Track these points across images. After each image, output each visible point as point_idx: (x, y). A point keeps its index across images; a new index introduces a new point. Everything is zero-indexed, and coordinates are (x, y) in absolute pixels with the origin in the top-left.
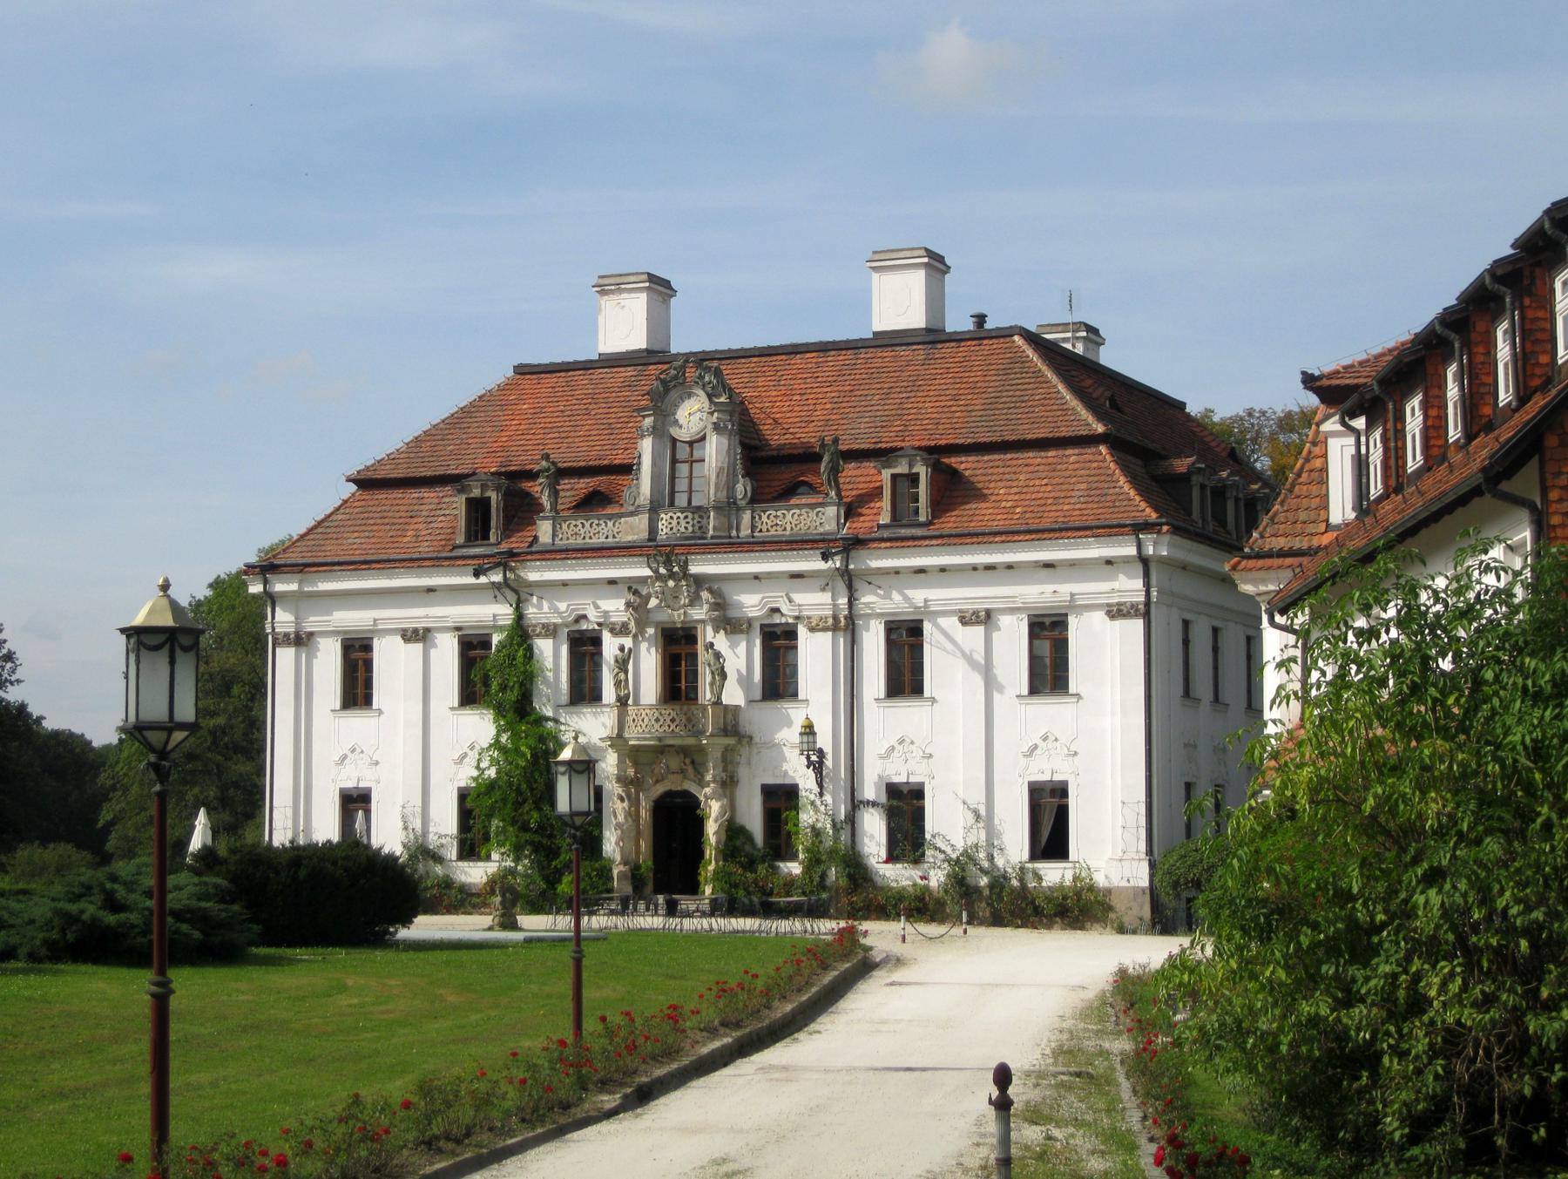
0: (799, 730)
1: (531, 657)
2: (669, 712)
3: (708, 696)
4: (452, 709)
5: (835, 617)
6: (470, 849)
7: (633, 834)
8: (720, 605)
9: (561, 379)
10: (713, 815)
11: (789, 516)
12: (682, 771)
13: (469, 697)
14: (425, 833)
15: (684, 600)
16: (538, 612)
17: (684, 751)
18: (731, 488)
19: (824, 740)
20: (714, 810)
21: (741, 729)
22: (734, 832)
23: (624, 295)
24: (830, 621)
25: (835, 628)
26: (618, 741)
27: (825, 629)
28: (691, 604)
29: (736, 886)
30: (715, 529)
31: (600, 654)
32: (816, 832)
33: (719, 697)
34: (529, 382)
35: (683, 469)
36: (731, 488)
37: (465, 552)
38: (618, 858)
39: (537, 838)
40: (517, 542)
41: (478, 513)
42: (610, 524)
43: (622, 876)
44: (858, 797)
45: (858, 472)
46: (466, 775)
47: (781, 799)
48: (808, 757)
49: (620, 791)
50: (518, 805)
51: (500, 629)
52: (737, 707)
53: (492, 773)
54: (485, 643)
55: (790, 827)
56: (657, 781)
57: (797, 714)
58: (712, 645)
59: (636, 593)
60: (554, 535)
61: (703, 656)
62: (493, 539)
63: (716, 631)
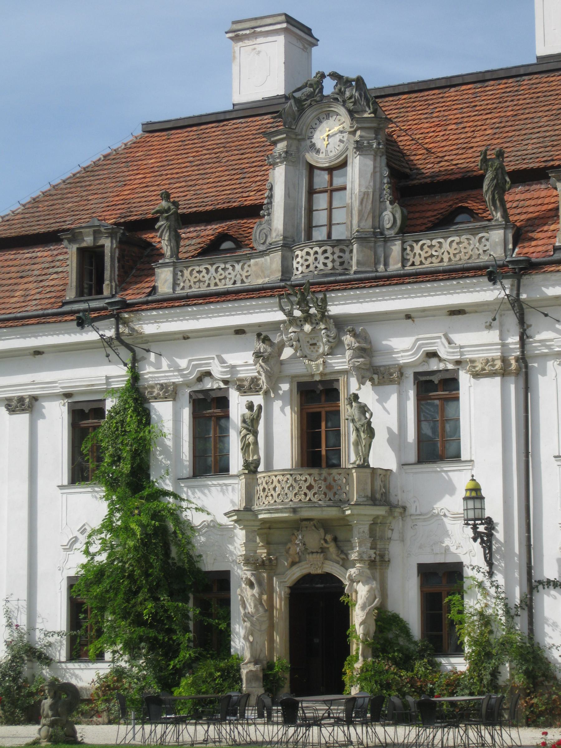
0: (463, 494)
1: (148, 423)
2: (307, 477)
3: (353, 458)
4: (61, 487)
5: (504, 360)
6: (80, 648)
7: (265, 626)
8: (366, 351)
9: (193, 132)
10: (360, 602)
11: (446, 246)
12: (323, 550)
13: (79, 474)
14: (31, 628)
15: (323, 348)
16: (157, 370)
17: (325, 525)
18: (377, 216)
19: (494, 508)
20: (361, 596)
21: (393, 500)
22: (385, 621)
23: (260, 40)
24: (498, 364)
25: (504, 373)
26: (245, 514)
27: (492, 374)
28: (331, 353)
29: (388, 686)
30: (358, 263)
31: (227, 417)
32: (486, 620)
33: (366, 459)
34: (156, 139)
35: (321, 201)
36: (377, 216)
37: (76, 307)
38: (247, 655)
39: (152, 633)
40: (132, 295)
41: (91, 259)
42: (238, 267)
43: (252, 676)
44: (536, 576)
45: (528, 195)
46: (76, 562)
47: (440, 581)
48: (475, 527)
49: (249, 574)
50: (132, 593)
51: (112, 392)
52: (388, 471)
53: (102, 558)
54: (98, 411)
55: (453, 615)
56: (293, 564)
57: (460, 478)
58: (356, 397)
59: (266, 340)
60: (175, 284)
61: (346, 411)
62: (106, 292)
63: (362, 382)
